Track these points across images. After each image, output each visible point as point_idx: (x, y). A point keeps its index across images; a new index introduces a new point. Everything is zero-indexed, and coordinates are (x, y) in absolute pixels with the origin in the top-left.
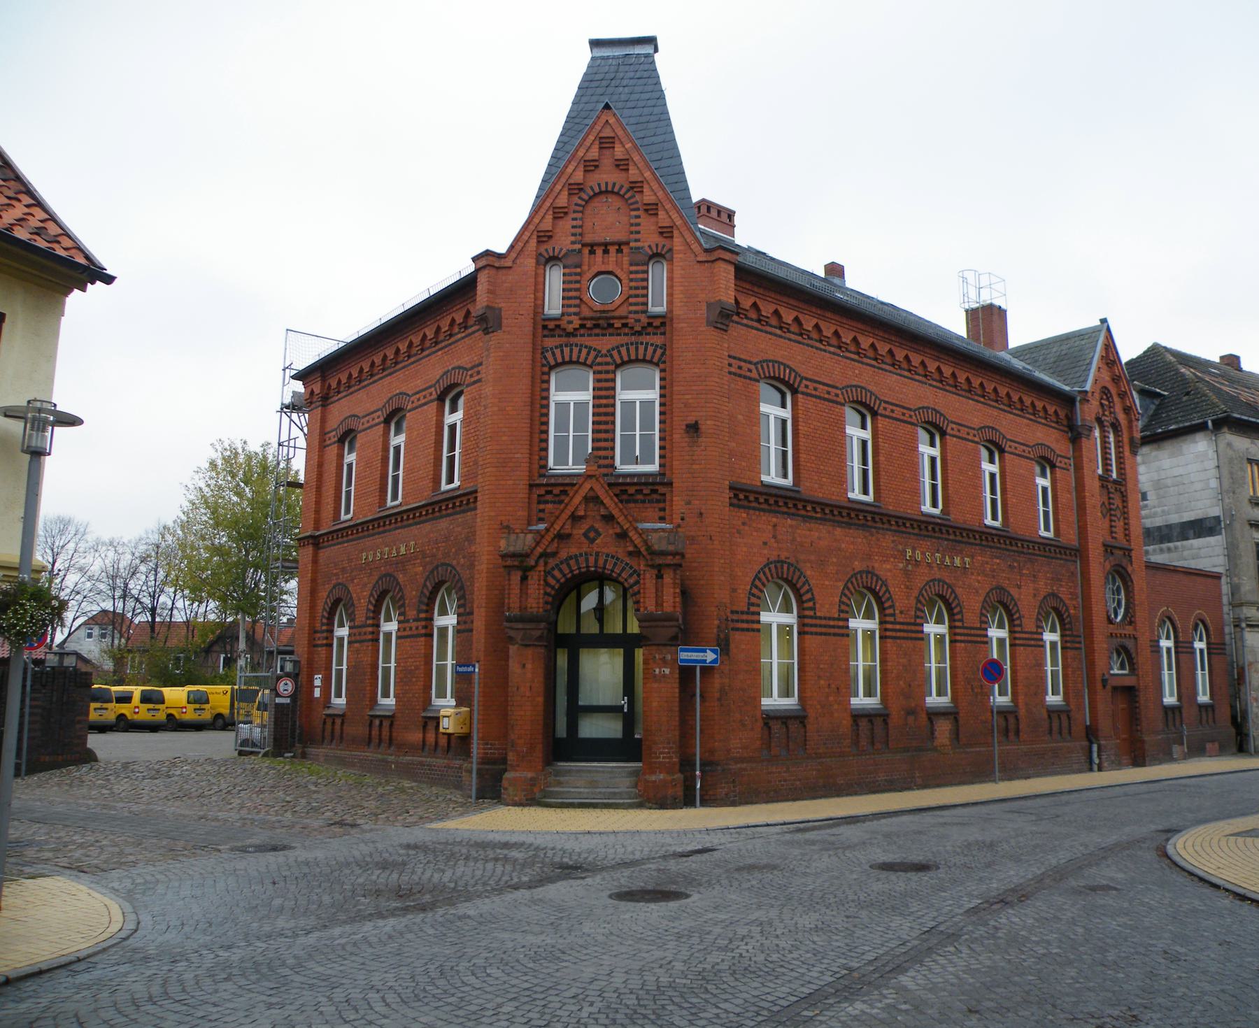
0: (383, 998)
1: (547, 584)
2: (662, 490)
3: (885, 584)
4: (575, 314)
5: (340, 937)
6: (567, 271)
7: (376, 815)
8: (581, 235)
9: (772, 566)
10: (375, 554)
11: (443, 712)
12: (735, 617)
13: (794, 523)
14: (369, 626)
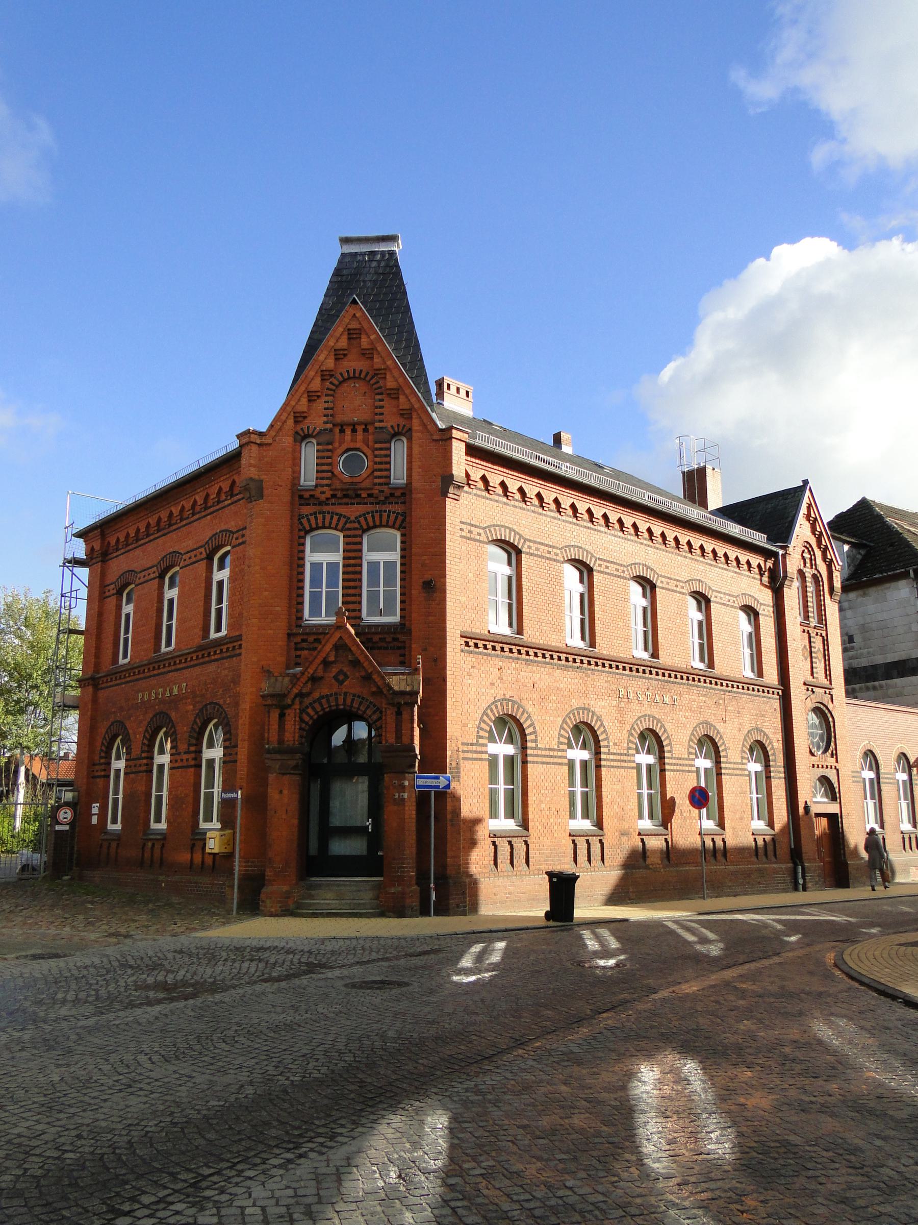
0: (150, 1059)
1: (302, 720)
2: (402, 638)
3: (599, 719)
4: (327, 485)
5: (115, 1019)
6: (320, 447)
7: (147, 927)
8: (331, 415)
9: (499, 704)
10: (150, 695)
11: (209, 834)
12: (465, 748)
13: (518, 666)
14: (145, 758)
